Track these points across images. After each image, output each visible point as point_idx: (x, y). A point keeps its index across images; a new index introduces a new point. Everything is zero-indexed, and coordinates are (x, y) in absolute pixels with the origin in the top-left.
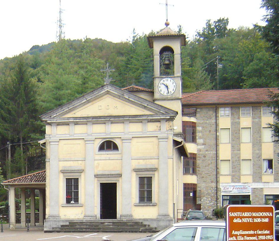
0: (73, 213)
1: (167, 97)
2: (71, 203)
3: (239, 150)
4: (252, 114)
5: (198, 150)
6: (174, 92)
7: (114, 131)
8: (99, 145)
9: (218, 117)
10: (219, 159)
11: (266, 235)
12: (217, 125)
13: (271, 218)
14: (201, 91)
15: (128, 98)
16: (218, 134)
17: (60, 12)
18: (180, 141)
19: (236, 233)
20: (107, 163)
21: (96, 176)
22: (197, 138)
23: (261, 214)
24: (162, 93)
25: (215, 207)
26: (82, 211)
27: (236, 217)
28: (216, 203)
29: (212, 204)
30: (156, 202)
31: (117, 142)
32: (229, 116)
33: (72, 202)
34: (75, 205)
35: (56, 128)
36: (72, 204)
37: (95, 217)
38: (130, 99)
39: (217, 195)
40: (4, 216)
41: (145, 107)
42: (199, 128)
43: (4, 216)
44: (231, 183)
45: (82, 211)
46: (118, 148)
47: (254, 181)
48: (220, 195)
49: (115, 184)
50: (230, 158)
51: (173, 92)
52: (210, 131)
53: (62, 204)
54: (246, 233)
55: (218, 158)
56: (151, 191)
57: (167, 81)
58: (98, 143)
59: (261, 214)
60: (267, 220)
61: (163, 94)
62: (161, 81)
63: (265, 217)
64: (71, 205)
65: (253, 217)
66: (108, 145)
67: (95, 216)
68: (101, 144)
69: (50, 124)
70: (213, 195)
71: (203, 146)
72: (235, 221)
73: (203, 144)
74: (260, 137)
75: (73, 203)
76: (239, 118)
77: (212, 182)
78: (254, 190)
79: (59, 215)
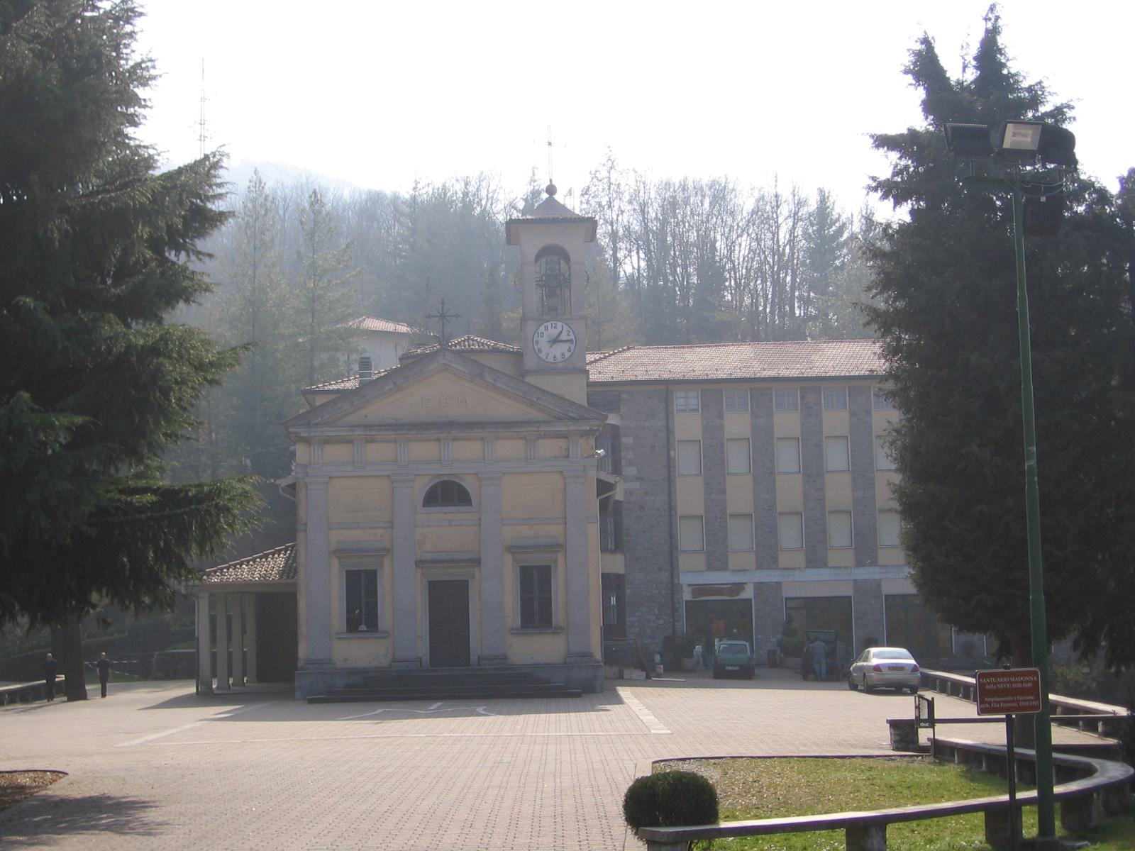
0: (362, 653)
1: (554, 365)
2: (359, 629)
3: (724, 492)
4: (752, 406)
5: (626, 493)
6: (571, 356)
7: (463, 457)
8: (426, 491)
9: (673, 413)
10: (676, 513)
11: (1029, 701)
12: (669, 431)
13: (1035, 683)
14: (625, 348)
15: (492, 381)
16: (672, 453)
17: (203, 100)
18: (613, 482)
19: (989, 699)
20: (445, 532)
21: (419, 563)
22: (623, 462)
23: (1022, 679)
24: (543, 356)
25: (671, 631)
26: (388, 649)
27: (989, 684)
28: (671, 620)
29: (661, 622)
30: (562, 625)
31: (470, 484)
32: (697, 410)
33: (363, 628)
34: (368, 635)
35: (320, 451)
36: (361, 631)
37: (419, 663)
38: (499, 385)
39: (673, 601)
40: (134, 662)
41: (532, 404)
42: (627, 441)
43: (134, 662)
44: (707, 570)
45: (388, 649)
46: (471, 500)
47: (760, 567)
48: (680, 600)
49: (464, 585)
50: (701, 511)
51: (569, 354)
52: (653, 447)
53: (338, 633)
54: (1002, 699)
55: (673, 513)
56: (366, 571)
57: (555, 327)
58: (422, 485)
59: (1022, 679)
60: (1030, 685)
61: (544, 358)
62: (541, 328)
63: (1028, 682)
64: (360, 635)
65: (1011, 683)
66: (447, 493)
67: (419, 660)
68: (431, 488)
69: (307, 441)
70: (663, 600)
71: (638, 485)
72: (987, 687)
73: (638, 479)
74: (772, 461)
75: (362, 629)
76: (721, 416)
77: (660, 570)
78: (759, 587)
79: (331, 660)
